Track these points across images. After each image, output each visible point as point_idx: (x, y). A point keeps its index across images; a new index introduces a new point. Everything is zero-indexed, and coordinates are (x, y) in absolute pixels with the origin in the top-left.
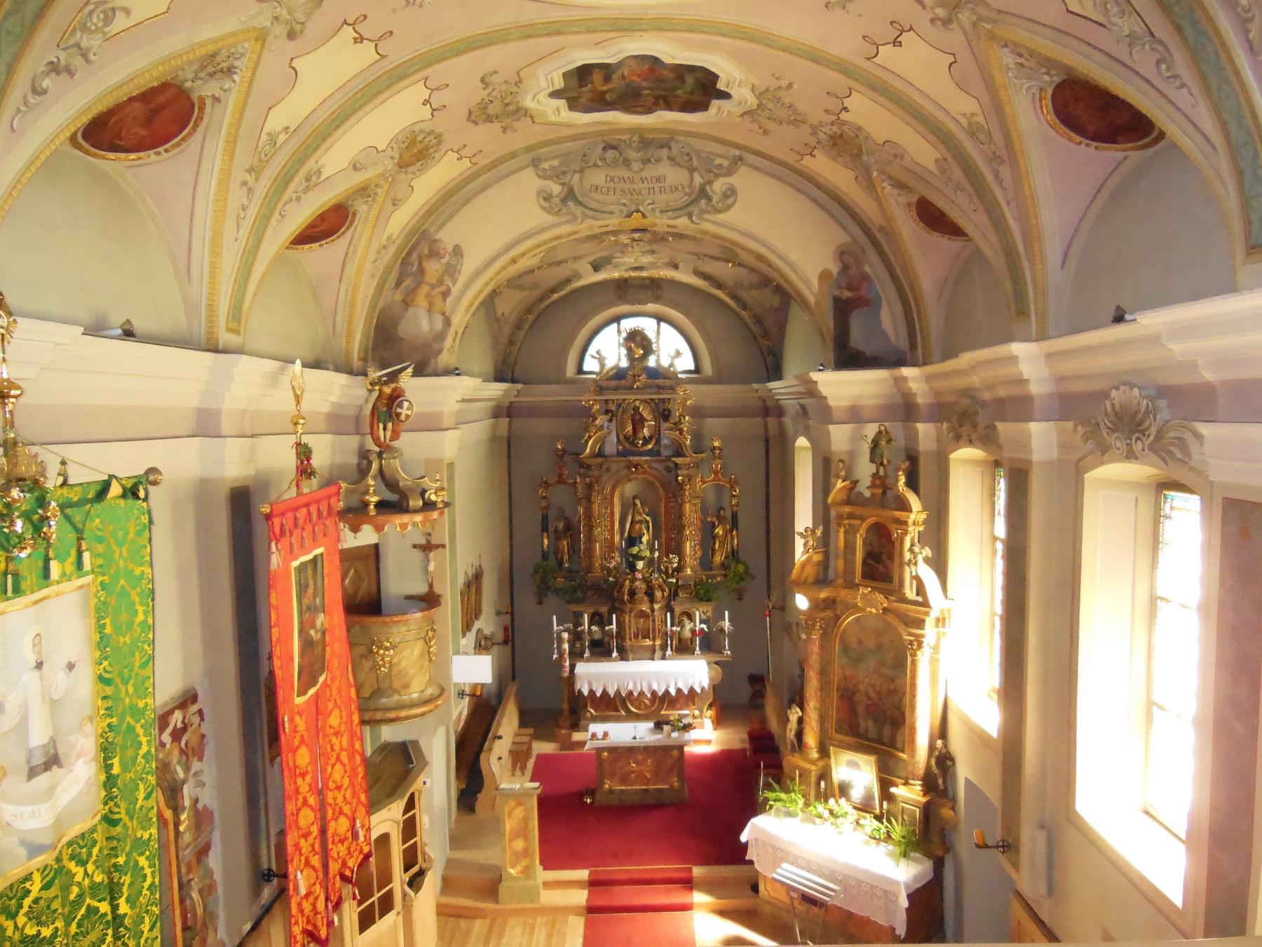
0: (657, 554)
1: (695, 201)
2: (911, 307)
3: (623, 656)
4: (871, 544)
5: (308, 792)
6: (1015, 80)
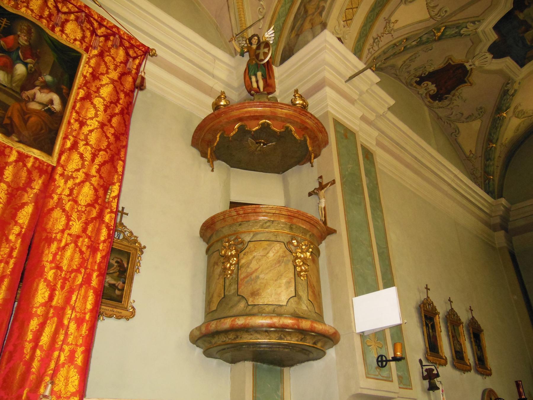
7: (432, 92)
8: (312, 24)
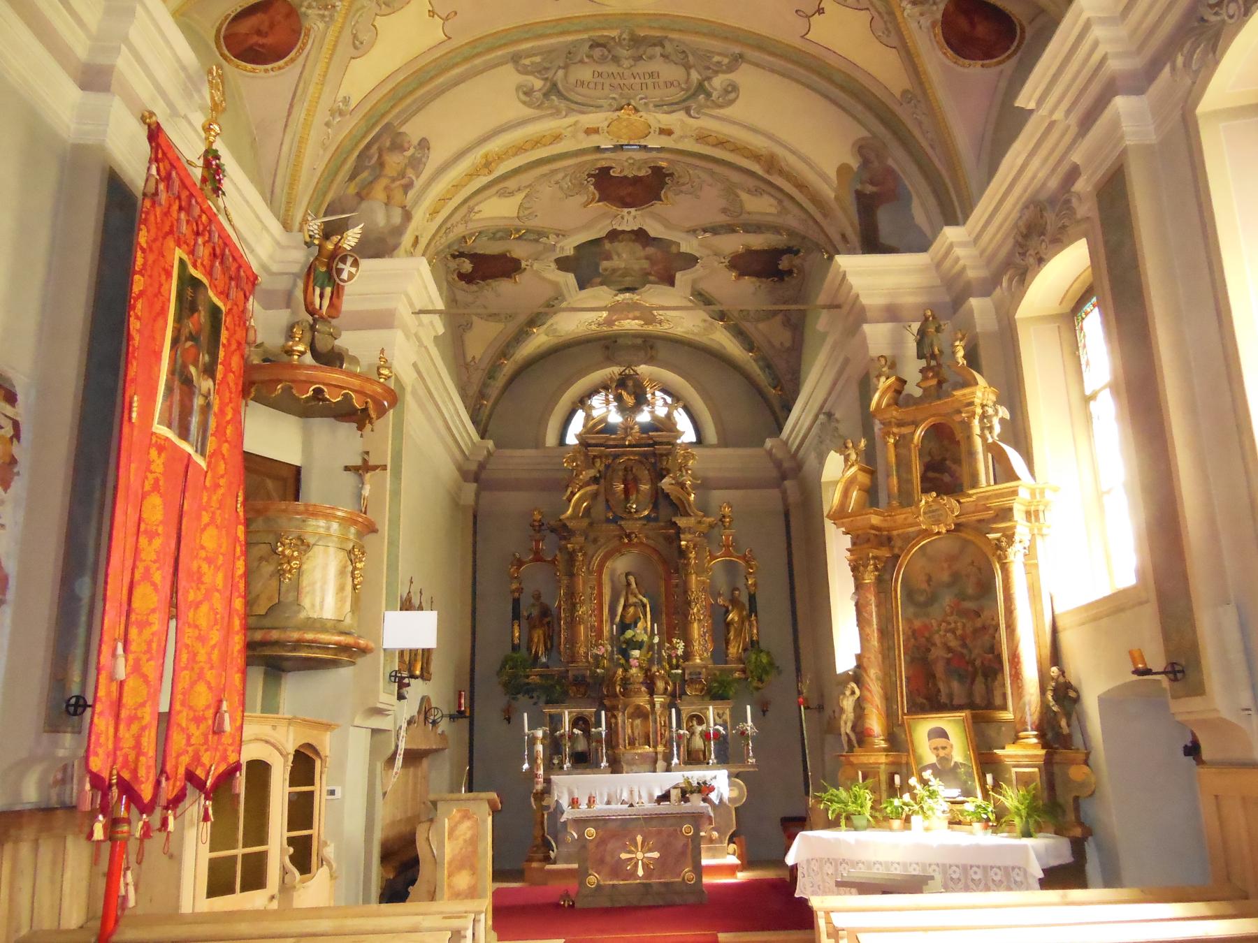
0: (656, 640)
1: (694, 95)
2: (944, 184)
3: (615, 766)
4: (930, 454)
5: (155, 562)
7: (463, 271)
8: (388, 197)
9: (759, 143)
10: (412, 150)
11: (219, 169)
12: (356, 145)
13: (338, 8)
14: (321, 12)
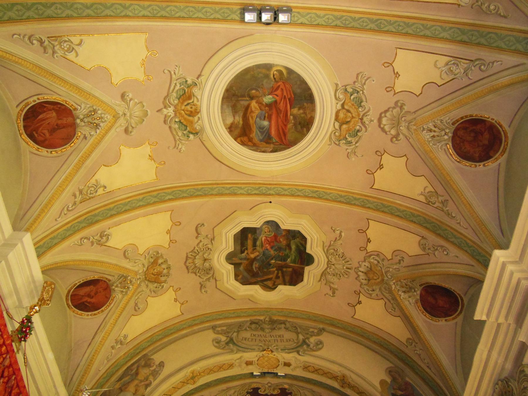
1: (301, 346)
6: (434, 146)
8: (136, 390)
9: (335, 369)
10: (155, 367)
11: (30, 328)
12: (127, 362)
13: (130, 289)
14: (122, 290)
